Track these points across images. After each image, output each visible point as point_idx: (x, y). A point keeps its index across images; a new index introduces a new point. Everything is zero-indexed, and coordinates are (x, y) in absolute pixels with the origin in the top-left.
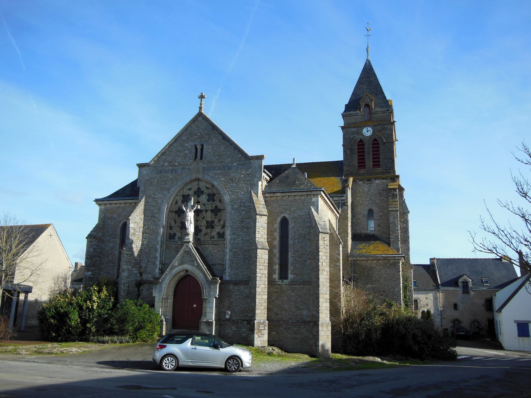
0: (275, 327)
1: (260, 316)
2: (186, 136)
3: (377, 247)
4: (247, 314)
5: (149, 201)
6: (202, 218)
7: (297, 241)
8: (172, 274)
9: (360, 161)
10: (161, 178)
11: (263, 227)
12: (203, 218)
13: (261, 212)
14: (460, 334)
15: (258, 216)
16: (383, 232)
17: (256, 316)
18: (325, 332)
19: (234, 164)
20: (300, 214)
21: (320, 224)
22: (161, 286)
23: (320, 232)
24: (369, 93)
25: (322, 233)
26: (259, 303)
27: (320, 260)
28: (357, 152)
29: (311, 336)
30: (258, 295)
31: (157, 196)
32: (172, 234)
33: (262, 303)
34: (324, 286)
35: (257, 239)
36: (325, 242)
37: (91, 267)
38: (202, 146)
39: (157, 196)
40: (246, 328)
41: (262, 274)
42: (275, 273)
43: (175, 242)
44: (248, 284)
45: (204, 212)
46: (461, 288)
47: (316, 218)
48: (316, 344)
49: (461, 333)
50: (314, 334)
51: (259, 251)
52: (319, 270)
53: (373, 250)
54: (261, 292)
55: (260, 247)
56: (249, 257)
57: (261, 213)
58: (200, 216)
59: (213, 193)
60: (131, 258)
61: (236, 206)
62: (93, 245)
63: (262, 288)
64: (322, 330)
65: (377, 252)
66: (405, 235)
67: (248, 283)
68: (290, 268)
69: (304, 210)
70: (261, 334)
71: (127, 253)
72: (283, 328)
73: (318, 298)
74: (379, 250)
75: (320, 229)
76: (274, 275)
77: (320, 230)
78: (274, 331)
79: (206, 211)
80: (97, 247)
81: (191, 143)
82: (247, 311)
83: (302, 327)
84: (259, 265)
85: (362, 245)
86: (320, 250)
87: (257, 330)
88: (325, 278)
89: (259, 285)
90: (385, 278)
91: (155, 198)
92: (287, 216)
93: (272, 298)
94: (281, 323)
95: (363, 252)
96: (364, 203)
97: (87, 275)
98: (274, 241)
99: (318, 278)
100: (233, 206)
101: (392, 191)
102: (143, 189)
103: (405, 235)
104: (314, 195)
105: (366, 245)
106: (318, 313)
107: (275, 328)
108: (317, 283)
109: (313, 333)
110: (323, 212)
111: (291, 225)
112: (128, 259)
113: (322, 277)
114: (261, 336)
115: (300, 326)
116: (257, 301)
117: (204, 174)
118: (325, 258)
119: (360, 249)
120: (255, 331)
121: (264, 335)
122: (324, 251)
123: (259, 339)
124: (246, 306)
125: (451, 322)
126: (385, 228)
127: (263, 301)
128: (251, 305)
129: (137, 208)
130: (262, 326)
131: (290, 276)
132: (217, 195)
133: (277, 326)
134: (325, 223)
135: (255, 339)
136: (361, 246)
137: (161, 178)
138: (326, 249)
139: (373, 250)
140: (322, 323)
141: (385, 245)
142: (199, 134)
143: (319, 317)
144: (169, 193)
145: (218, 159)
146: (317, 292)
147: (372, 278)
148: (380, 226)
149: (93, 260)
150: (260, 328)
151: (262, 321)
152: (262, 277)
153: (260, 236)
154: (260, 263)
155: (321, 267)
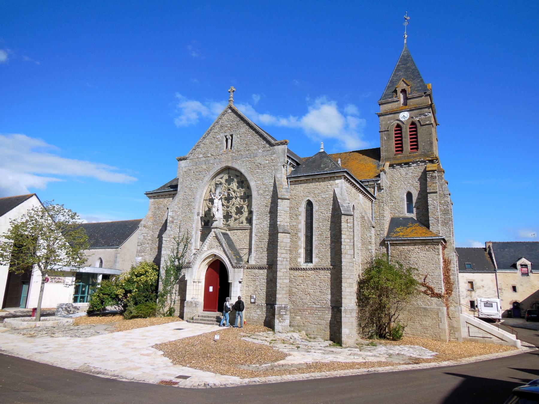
0: (300, 311)
1: (281, 300)
2: (218, 129)
3: (415, 229)
4: (270, 298)
5: (186, 191)
6: (232, 204)
7: (321, 224)
8: (202, 258)
9: (397, 146)
10: (196, 169)
11: (285, 210)
12: (233, 205)
13: (283, 196)
14: (531, 316)
15: (279, 200)
16: (422, 215)
17: (277, 300)
18: (349, 319)
19: (260, 151)
20: (324, 196)
21: (343, 206)
22: (192, 270)
23: (343, 215)
24: (406, 79)
25: (344, 215)
26: (280, 287)
27: (342, 243)
28: (394, 137)
29: (335, 322)
30: (280, 279)
31: (192, 186)
32: (206, 221)
33: (284, 287)
34: (347, 270)
35: (278, 223)
36: (348, 225)
37: (142, 253)
38: (232, 136)
39: (192, 186)
40: (270, 312)
41: (284, 258)
42: (300, 257)
43: (208, 228)
44: (272, 268)
45: (234, 199)
46: (520, 270)
47: (339, 200)
48: (339, 331)
49: (532, 315)
50: (338, 320)
51: (280, 235)
52: (341, 254)
53: (410, 233)
54: (282, 276)
55: (281, 231)
56: (273, 241)
57: (283, 197)
58: (230, 202)
59: (242, 180)
60: (169, 244)
61: (261, 192)
62: (143, 233)
63: (283, 272)
64: (345, 317)
65: (415, 235)
66: (445, 217)
67: (272, 267)
68: (315, 251)
69: (328, 193)
70: (282, 319)
71: (166, 239)
72: (307, 313)
73: (341, 282)
74: (417, 233)
75: (343, 210)
76: (299, 259)
77: (343, 212)
78: (299, 316)
79: (236, 198)
80: (146, 235)
81: (221, 134)
82: (271, 295)
83: (327, 312)
84: (280, 249)
85: (400, 228)
86: (342, 233)
87: (278, 315)
88: (348, 261)
89: (280, 269)
90: (423, 261)
91: (191, 188)
92: (312, 200)
93: (297, 283)
94: (305, 308)
95: (399, 235)
96: (402, 186)
97: (138, 260)
98: (299, 225)
99: (341, 262)
100: (259, 192)
101: (431, 172)
102: (182, 181)
103: (445, 217)
104: (337, 176)
105: (404, 228)
106: (341, 298)
107: (300, 312)
108: (340, 266)
109: (337, 319)
110: (350, 194)
111: (315, 208)
112: (167, 245)
113: (345, 261)
114: (282, 321)
115: (324, 312)
116: (278, 285)
117: (233, 163)
118: (349, 241)
119: (397, 232)
120: (276, 316)
121: (285, 320)
122: (347, 233)
123: (280, 325)
124: (270, 290)
125: (510, 304)
126: (424, 210)
127: (284, 285)
128: (274, 289)
129: (176, 198)
130: (283, 311)
131: (314, 259)
132: (245, 182)
133: (302, 310)
134: (349, 205)
135: (276, 324)
136: (398, 229)
137: (196, 169)
138: (350, 232)
139: (410, 233)
140: (345, 309)
141: (423, 227)
142: (229, 125)
143: (341, 303)
144: (203, 182)
145: (245, 147)
146: (340, 276)
147: (409, 262)
148: (419, 208)
149: (143, 247)
150: (281, 313)
151: (283, 306)
152: (283, 261)
153: (282, 219)
154: (281, 247)
155: (344, 251)
